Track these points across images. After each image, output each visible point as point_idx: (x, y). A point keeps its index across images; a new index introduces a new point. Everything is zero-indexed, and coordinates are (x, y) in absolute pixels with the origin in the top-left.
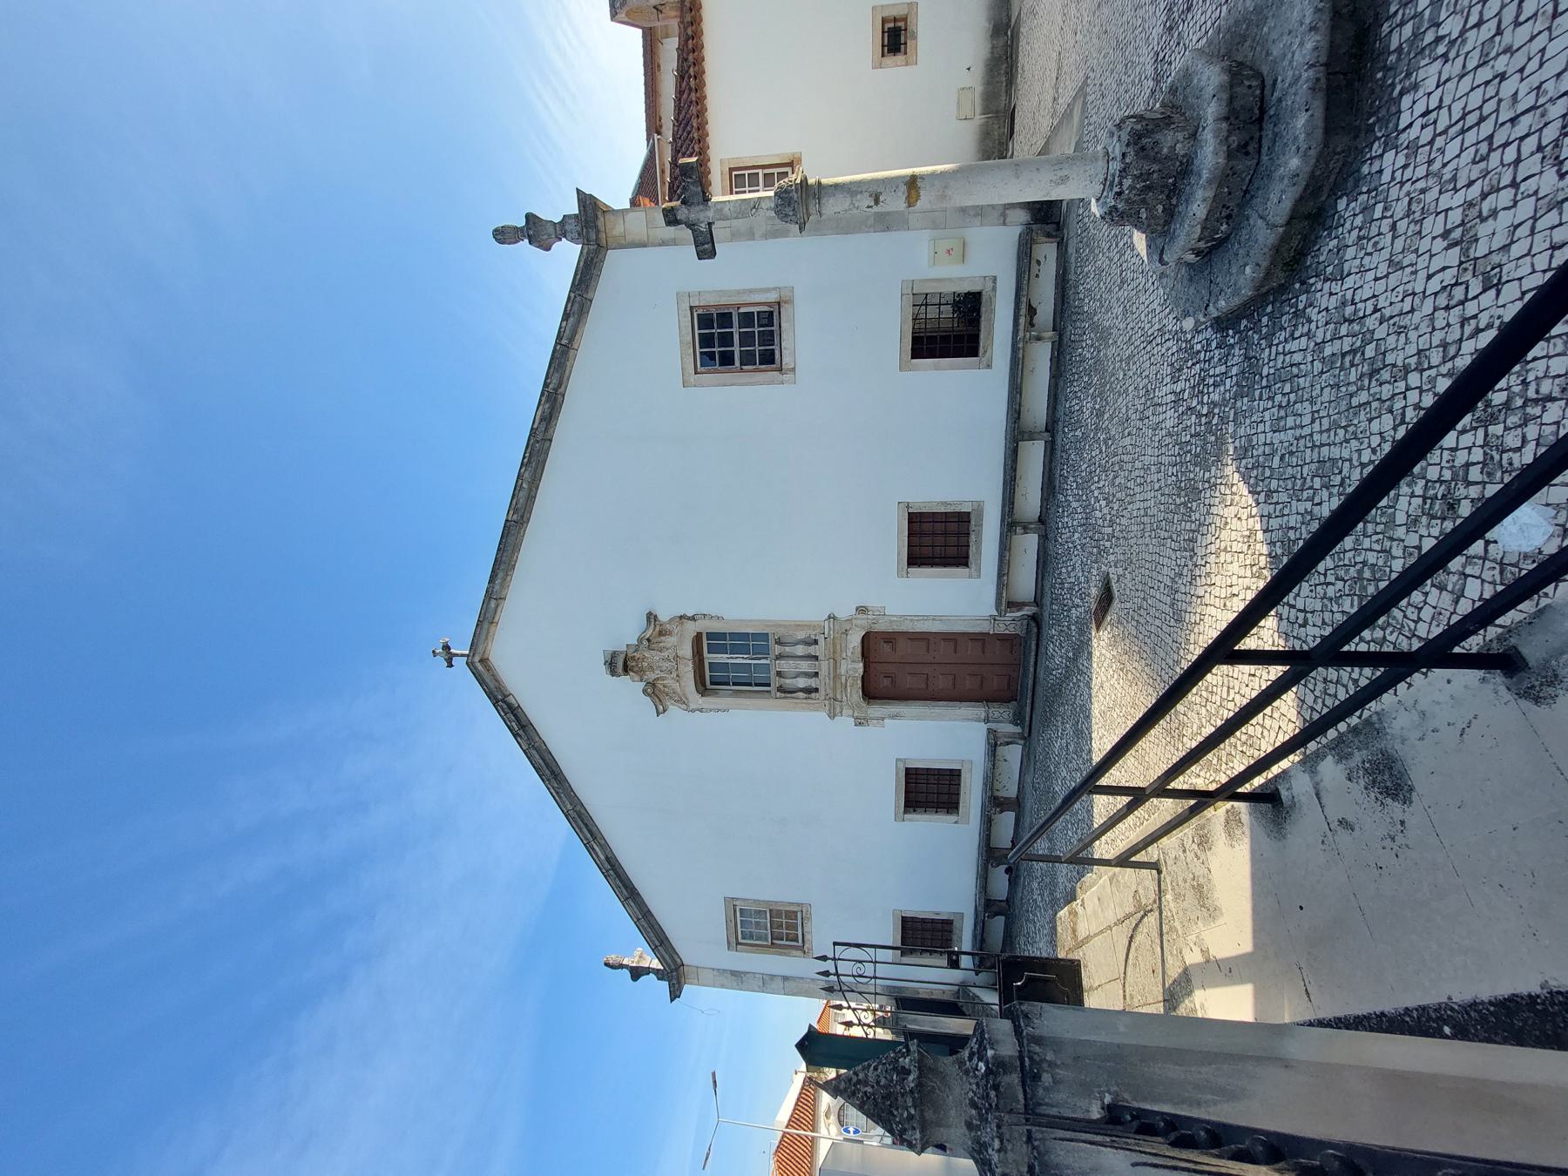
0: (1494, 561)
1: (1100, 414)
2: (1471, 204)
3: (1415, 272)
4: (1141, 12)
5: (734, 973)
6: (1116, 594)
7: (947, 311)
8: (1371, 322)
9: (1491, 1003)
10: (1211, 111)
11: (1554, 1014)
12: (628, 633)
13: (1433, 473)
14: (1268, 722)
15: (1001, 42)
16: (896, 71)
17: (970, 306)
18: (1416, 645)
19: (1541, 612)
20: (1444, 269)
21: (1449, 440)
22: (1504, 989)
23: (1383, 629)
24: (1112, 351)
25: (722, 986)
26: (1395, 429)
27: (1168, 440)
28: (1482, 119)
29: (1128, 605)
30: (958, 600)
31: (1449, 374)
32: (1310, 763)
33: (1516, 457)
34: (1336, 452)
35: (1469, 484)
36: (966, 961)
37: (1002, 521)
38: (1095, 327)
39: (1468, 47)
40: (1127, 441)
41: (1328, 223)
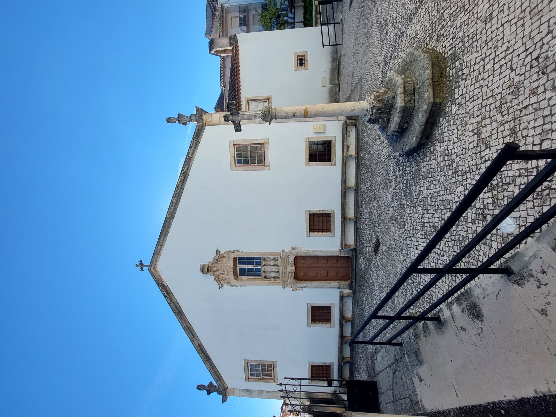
0: (500, 236)
1: (372, 181)
2: (478, 123)
3: (465, 142)
4: (377, 58)
5: (247, 391)
6: (381, 243)
7: (320, 147)
8: (454, 156)
9: (515, 401)
10: (400, 90)
11: (537, 406)
12: (208, 258)
13: (478, 206)
14: (434, 290)
15: (335, 63)
16: (302, 72)
17: (328, 145)
18: (480, 264)
19: (515, 254)
20: (473, 141)
21: (481, 195)
22: (519, 396)
23: (469, 258)
24: (374, 161)
25: (243, 396)
26: (465, 191)
27: (394, 191)
28: (478, 98)
29: (385, 247)
30: (328, 244)
31: (479, 174)
32: (449, 306)
33: (502, 202)
34: (447, 197)
35: (489, 210)
36: (335, 384)
37: (342, 216)
38: (368, 153)
39: (472, 77)
40: (381, 191)
41: (438, 125)
